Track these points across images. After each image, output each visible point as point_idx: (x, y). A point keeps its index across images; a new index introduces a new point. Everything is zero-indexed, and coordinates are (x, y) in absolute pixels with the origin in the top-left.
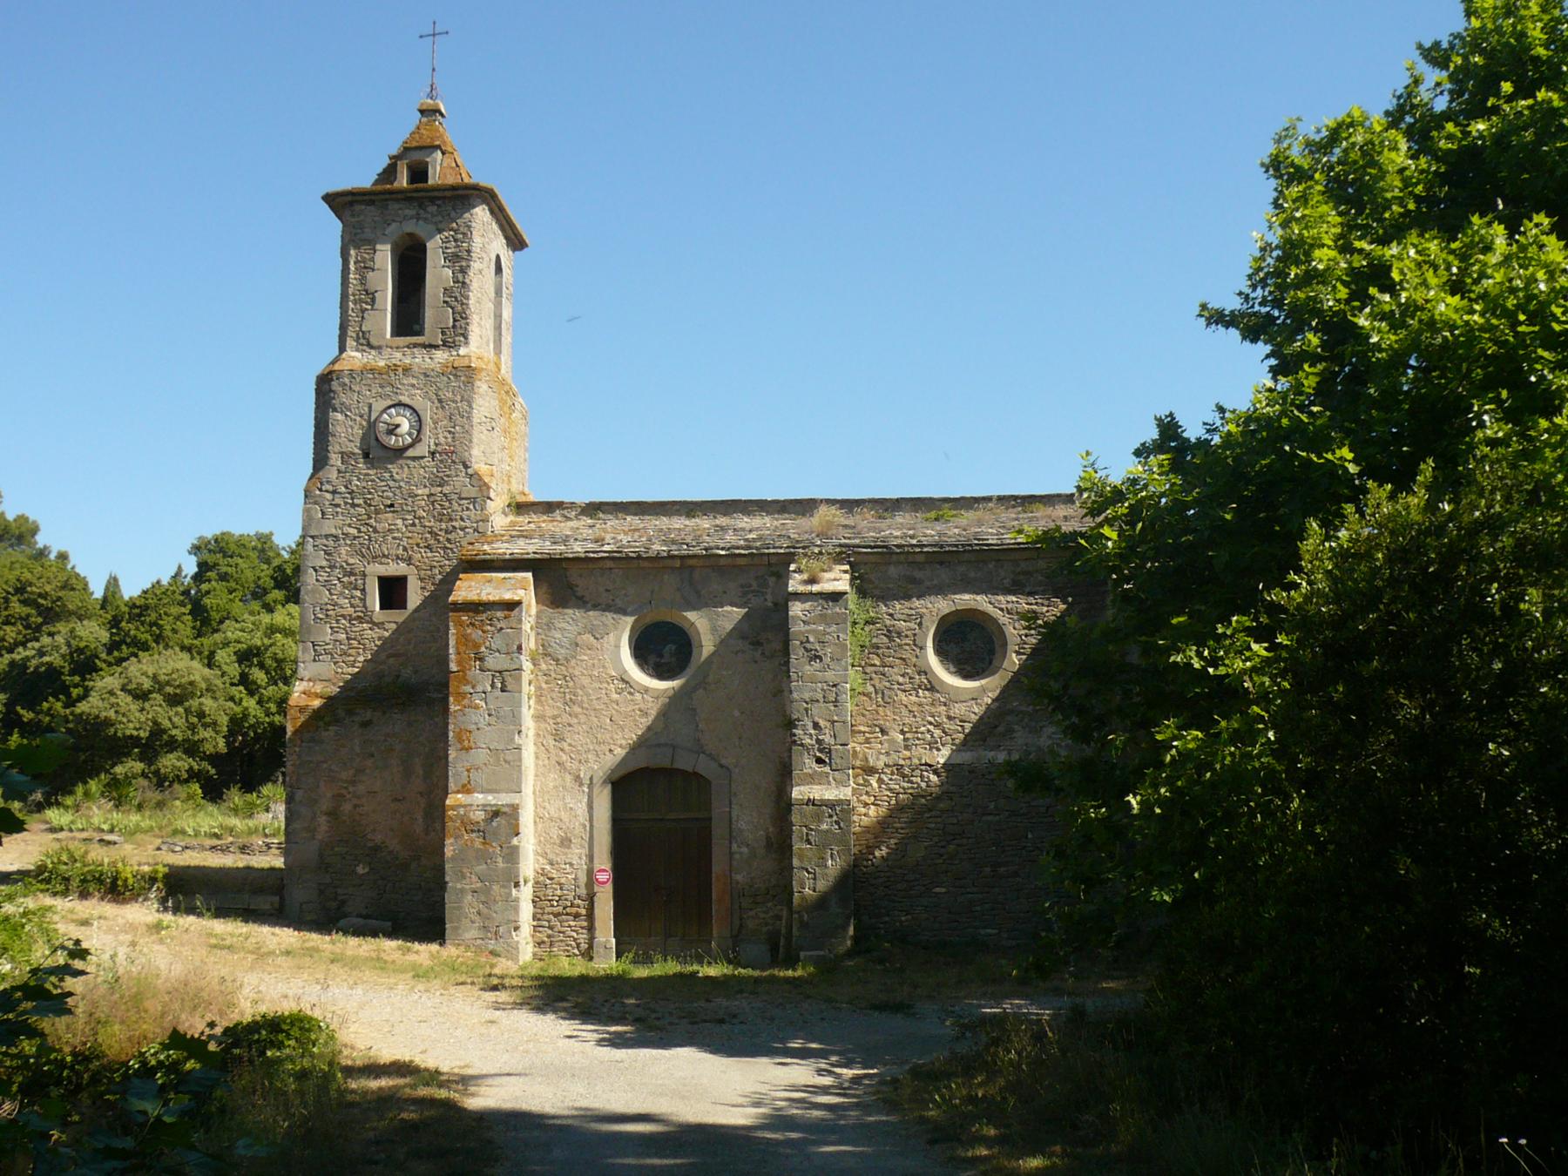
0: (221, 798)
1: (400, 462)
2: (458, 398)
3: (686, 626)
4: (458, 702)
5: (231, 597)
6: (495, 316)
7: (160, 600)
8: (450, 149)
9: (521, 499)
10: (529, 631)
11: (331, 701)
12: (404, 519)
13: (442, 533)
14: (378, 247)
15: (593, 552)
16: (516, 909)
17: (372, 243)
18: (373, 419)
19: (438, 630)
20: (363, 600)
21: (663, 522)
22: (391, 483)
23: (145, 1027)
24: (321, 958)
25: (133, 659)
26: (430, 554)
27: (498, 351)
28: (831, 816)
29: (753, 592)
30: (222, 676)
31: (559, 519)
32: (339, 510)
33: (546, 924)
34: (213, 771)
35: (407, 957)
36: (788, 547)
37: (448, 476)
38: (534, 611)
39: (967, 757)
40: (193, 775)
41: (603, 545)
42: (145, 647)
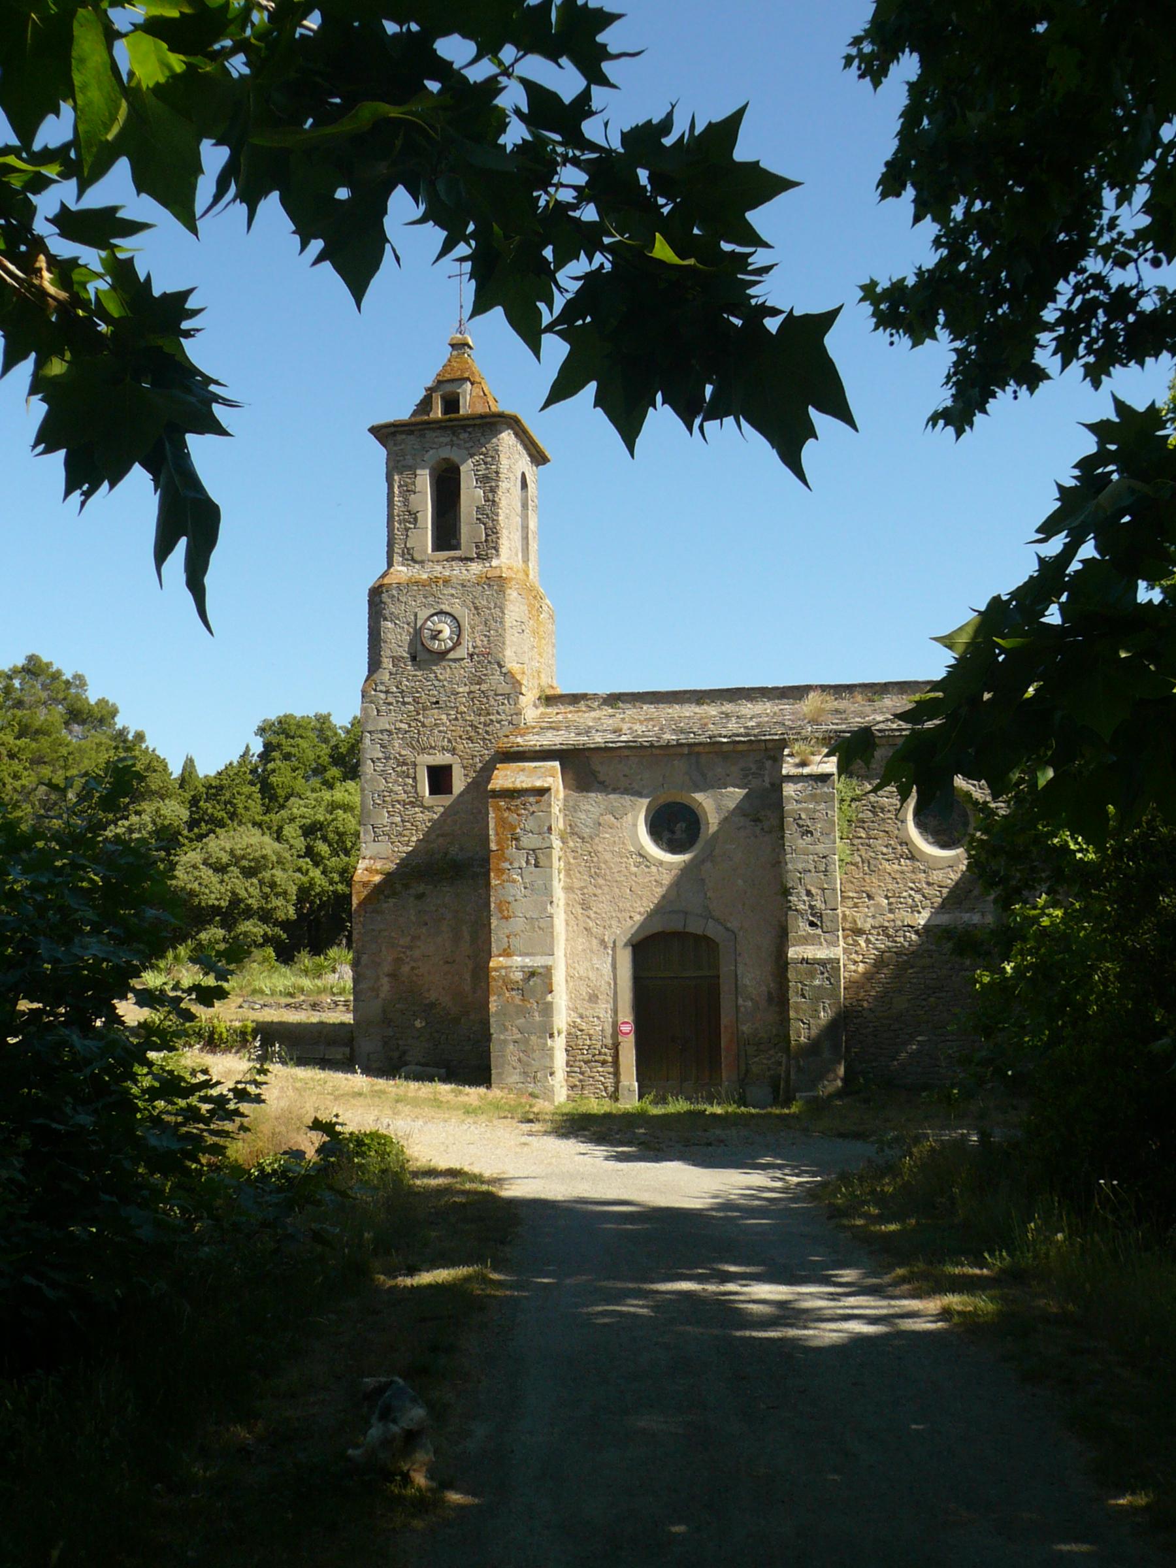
0: (292, 960)
1: (444, 663)
2: (492, 605)
3: (694, 806)
4: (498, 877)
5: (294, 774)
6: (522, 527)
7: (233, 780)
8: (478, 380)
9: (550, 692)
10: (558, 813)
11: (389, 877)
12: (448, 715)
13: (481, 726)
14: (419, 472)
15: (612, 742)
16: (551, 1057)
17: (413, 469)
18: (418, 626)
19: (480, 812)
20: (415, 787)
21: (675, 711)
22: (436, 683)
23: (261, 1144)
24: (387, 1099)
25: (212, 835)
26: (471, 745)
27: (526, 560)
28: (822, 973)
29: (753, 774)
30: (290, 849)
31: (584, 709)
32: (391, 707)
33: (577, 1070)
34: (284, 936)
35: (459, 1098)
36: (782, 734)
37: (485, 675)
38: (561, 795)
39: (944, 919)
40: (267, 940)
41: (620, 736)
42: (221, 824)
